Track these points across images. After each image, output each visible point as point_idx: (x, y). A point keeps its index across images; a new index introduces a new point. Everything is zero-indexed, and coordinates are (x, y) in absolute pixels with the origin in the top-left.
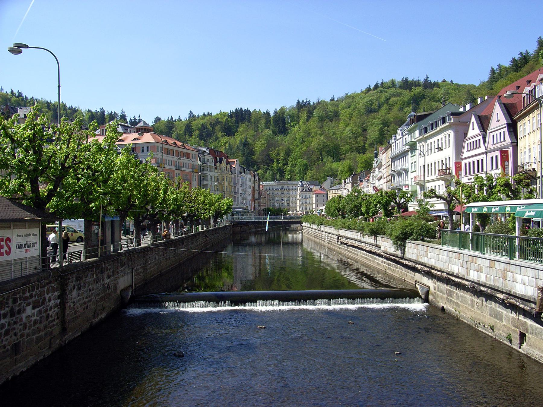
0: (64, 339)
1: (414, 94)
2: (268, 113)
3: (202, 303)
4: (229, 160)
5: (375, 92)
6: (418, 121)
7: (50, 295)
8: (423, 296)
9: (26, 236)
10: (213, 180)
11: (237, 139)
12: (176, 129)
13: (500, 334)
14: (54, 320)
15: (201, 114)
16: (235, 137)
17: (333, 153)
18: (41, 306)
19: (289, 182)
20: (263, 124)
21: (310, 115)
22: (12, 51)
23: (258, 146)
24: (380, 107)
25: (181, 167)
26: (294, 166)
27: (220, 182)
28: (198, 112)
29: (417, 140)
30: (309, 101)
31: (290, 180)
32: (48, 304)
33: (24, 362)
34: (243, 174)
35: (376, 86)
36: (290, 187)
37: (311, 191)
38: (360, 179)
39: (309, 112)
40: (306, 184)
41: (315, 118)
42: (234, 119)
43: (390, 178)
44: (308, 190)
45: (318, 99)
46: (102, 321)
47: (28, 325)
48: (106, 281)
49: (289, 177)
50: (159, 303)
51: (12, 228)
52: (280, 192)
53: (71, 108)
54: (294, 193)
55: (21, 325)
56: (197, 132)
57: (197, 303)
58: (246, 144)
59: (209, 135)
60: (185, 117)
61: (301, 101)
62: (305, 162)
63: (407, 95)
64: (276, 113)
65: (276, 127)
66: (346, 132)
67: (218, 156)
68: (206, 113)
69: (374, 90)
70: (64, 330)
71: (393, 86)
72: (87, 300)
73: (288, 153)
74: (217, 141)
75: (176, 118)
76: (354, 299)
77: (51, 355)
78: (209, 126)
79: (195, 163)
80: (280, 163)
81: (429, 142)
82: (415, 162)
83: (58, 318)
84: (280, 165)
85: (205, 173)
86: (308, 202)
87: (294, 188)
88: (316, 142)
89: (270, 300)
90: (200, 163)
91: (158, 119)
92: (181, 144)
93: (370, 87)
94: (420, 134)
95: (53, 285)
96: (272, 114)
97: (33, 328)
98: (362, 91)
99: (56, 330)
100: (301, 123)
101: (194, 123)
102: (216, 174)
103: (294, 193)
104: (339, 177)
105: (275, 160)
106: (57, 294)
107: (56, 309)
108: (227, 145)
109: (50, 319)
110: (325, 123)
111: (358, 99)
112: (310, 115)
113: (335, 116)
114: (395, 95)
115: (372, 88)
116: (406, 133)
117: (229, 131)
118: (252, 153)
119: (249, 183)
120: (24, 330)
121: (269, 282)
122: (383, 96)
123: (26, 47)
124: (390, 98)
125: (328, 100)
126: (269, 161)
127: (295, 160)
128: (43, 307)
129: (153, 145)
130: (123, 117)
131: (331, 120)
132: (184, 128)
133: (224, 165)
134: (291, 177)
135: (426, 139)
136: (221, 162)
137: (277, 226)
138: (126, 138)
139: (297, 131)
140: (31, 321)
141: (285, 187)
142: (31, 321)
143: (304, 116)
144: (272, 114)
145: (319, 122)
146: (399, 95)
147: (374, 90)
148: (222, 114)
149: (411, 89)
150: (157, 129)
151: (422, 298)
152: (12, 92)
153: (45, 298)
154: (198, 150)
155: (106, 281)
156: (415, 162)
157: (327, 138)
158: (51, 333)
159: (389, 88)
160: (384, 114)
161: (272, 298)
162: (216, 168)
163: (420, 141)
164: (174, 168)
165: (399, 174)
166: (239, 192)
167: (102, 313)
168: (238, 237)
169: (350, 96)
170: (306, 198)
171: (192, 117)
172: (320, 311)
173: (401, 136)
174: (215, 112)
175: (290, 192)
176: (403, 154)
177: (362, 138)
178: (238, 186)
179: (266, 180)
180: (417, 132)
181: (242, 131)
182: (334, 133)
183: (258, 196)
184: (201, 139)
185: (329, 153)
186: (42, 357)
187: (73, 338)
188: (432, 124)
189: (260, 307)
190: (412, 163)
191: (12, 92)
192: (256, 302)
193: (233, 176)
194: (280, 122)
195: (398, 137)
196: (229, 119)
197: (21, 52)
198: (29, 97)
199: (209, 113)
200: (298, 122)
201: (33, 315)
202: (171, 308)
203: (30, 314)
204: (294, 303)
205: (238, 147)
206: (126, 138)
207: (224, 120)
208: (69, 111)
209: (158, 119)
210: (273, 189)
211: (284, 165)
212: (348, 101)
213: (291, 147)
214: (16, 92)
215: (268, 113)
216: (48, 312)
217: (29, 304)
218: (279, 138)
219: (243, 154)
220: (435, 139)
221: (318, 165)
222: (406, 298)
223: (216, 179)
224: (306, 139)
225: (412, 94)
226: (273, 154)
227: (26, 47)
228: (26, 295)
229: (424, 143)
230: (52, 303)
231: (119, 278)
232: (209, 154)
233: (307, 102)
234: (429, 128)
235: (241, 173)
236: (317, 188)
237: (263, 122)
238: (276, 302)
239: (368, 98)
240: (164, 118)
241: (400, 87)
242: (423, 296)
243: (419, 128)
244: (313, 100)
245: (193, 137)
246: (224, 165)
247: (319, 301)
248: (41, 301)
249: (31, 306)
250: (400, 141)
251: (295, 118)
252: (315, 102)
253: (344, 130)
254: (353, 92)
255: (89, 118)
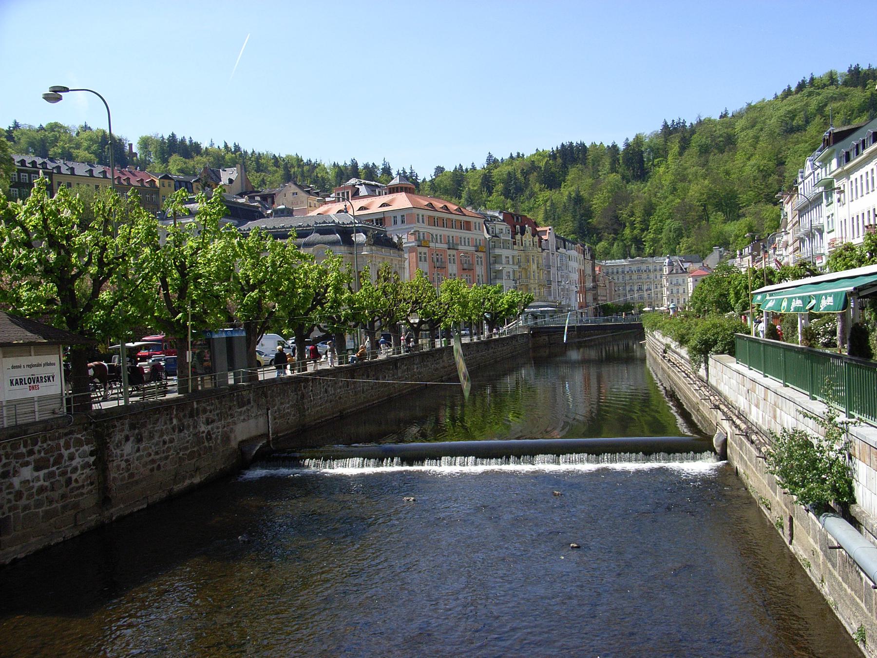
0: (107, 514)
1: (872, 94)
2: (614, 147)
3: (357, 460)
4: (538, 229)
5: (799, 95)
6: (835, 142)
7: (72, 450)
8: (718, 449)
9: (30, 366)
10: (511, 262)
11: (565, 192)
12: (468, 183)
13: (772, 516)
14: (83, 486)
15: (506, 157)
16: (562, 189)
17: (726, 206)
18: (53, 466)
19: (650, 259)
20: (608, 166)
21: (685, 145)
22: (47, 97)
23: (598, 202)
24: (807, 121)
25: (457, 244)
26: (659, 231)
27: (522, 264)
28: (502, 154)
29: (835, 177)
30: (684, 122)
31: (652, 255)
32: (67, 463)
33: (19, 546)
34: (562, 250)
35: (801, 86)
36: (651, 267)
37: (686, 272)
38: (764, 247)
39: (682, 139)
40: (676, 261)
41: (694, 149)
42: (559, 161)
43: (797, 244)
44: (680, 271)
45: (699, 117)
46: (191, 490)
47: (26, 494)
48: (203, 428)
49: (651, 251)
50: (296, 462)
51: (33, 353)
52: (635, 277)
53: (309, 163)
54: (658, 277)
55: (10, 493)
56: (500, 187)
57: (350, 461)
58: (578, 200)
59: (520, 190)
60: (481, 164)
61: (669, 123)
62: (676, 224)
63: (858, 96)
64: (628, 145)
65: (628, 169)
66: (748, 170)
67: (518, 223)
68: (515, 155)
69: (797, 92)
70: (105, 500)
71: (832, 84)
72: (158, 457)
73: (649, 210)
74: (533, 199)
75: (467, 165)
76: (598, 455)
77: (78, 536)
78: (519, 176)
79: (479, 237)
80: (635, 228)
81: (852, 177)
82: (832, 215)
83: (92, 484)
84: (635, 232)
85: (497, 251)
86: (681, 291)
87: (658, 268)
88: (695, 190)
89: (461, 456)
90: (487, 236)
91: (440, 170)
92: (456, 207)
93: (789, 88)
94: (839, 165)
95: (79, 436)
96: (621, 146)
97: (36, 497)
98: (776, 97)
99: (89, 500)
100: (670, 158)
101: (495, 172)
102: (516, 253)
103: (658, 277)
104: (731, 247)
105: (627, 224)
106: (87, 448)
107: (87, 471)
108: (548, 204)
109: (74, 484)
110: (711, 157)
111: (768, 112)
112: (685, 145)
113: (729, 142)
114: (835, 99)
115: (793, 89)
116: (818, 164)
117: (552, 181)
118: (589, 214)
119: (574, 265)
120: (16, 501)
121: (625, 424)
122: (814, 102)
123: (66, 90)
124: (826, 105)
125: (716, 117)
126: (617, 225)
127: (661, 221)
128: (58, 469)
129: (410, 212)
130: (387, 171)
131: (722, 151)
132: (480, 181)
133: (528, 237)
134: (654, 251)
135: (847, 174)
136: (523, 233)
137: (614, 335)
138: (370, 204)
139: (663, 173)
140: (33, 487)
141: (644, 267)
142: (33, 487)
143: (675, 148)
144: (621, 146)
145: (700, 156)
146: (843, 97)
147: (797, 92)
148: (539, 154)
149: (864, 86)
150: (439, 185)
151: (716, 453)
152: (226, 146)
153: (61, 456)
154: (485, 216)
155: (203, 428)
156: (832, 215)
157: (714, 181)
158: (76, 506)
159: (825, 85)
160: (815, 134)
161: (465, 452)
162: (515, 243)
163: (839, 177)
164: (446, 246)
165: (810, 235)
166: (561, 281)
167: (192, 476)
168: (544, 353)
169: (755, 107)
170: (678, 284)
171: (492, 162)
172: (537, 476)
173: (811, 171)
174: (528, 152)
175: (652, 276)
176: (816, 202)
177: (777, 177)
178: (553, 270)
179: (613, 258)
180: (834, 162)
181: (573, 179)
182: (727, 173)
183: (592, 286)
184: (507, 197)
185: (719, 207)
186: (61, 539)
187: (127, 512)
188: (857, 146)
189: (445, 468)
190: (828, 217)
191: (226, 146)
192: (440, 459)
193: (544, 254)
194: (635, 160)
195: (807, 173)
196: (551, 162)
197: (60, 98)
198: (250, 152)
199: (518, 153)
200: (666, 158)
201: (38, 479)
202: (313, 469)
203: (29, 478)
204: (499, 460)
205: (565, 206)
206: (370, 204)
207: (542, 164)
208: (306, 168)
209: (440, 170)
210: (623, 272)
211: (643, 230)
212: (755, 114)
213: (654, 200)
214: (231, 145)
215: (614, 147)
216: (69, 475)
217: (27, 464)
218: (633, 187)
219: (574, 217)
220: (862, 171)
221: (699, 228)
222: (688, 452)
223: (516, 261)
224: (680, 185)
225: (868, 93)
226: (624, 214)
227: (66, 90)
228: (19, 451)
229: (844, 180)
230: (77, 461)
231: (235, 423)
232: (503, 221)
233: (679, 123)
234: (852, 154)
235: (558, 248)
236: (697, 266)
237: (607, 162)
238: (471, 459)
239: (785, 108)
240: (449, 168)
241: (845, 84)
242: (718, 449)
243: (838, 154)
244: (690, 120)
245: (495, 194)
246: (528, 237)
247: (539, 458)
248: (52, 460)
249: (30, 467)
250: (809, 179)
251: (660, 152)
252: (695, 122)
253: (745, 165)
254: (760, 99)
255: (337, 177)
